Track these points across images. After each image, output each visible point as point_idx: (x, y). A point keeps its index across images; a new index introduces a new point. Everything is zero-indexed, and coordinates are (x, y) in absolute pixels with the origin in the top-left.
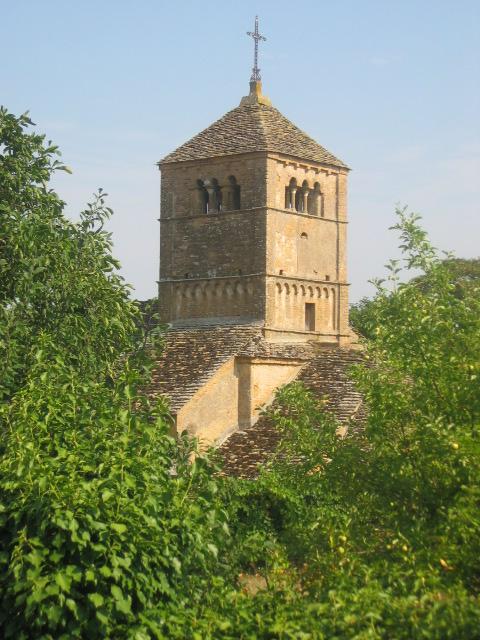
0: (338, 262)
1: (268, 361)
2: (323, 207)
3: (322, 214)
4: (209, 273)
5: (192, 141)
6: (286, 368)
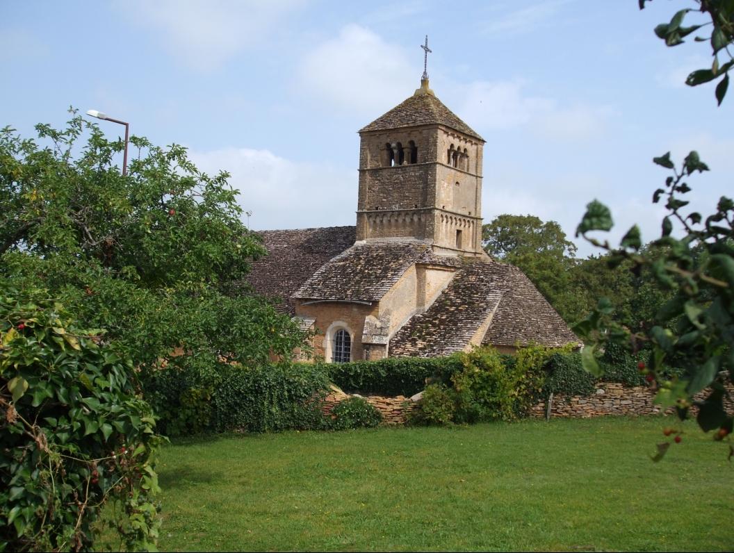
0: (476, 203)
1: (437, 268)
2: (468, 166)
3: (468, 170)
4: (394, 207)
5: (381, 118)
6: (447, 273)
